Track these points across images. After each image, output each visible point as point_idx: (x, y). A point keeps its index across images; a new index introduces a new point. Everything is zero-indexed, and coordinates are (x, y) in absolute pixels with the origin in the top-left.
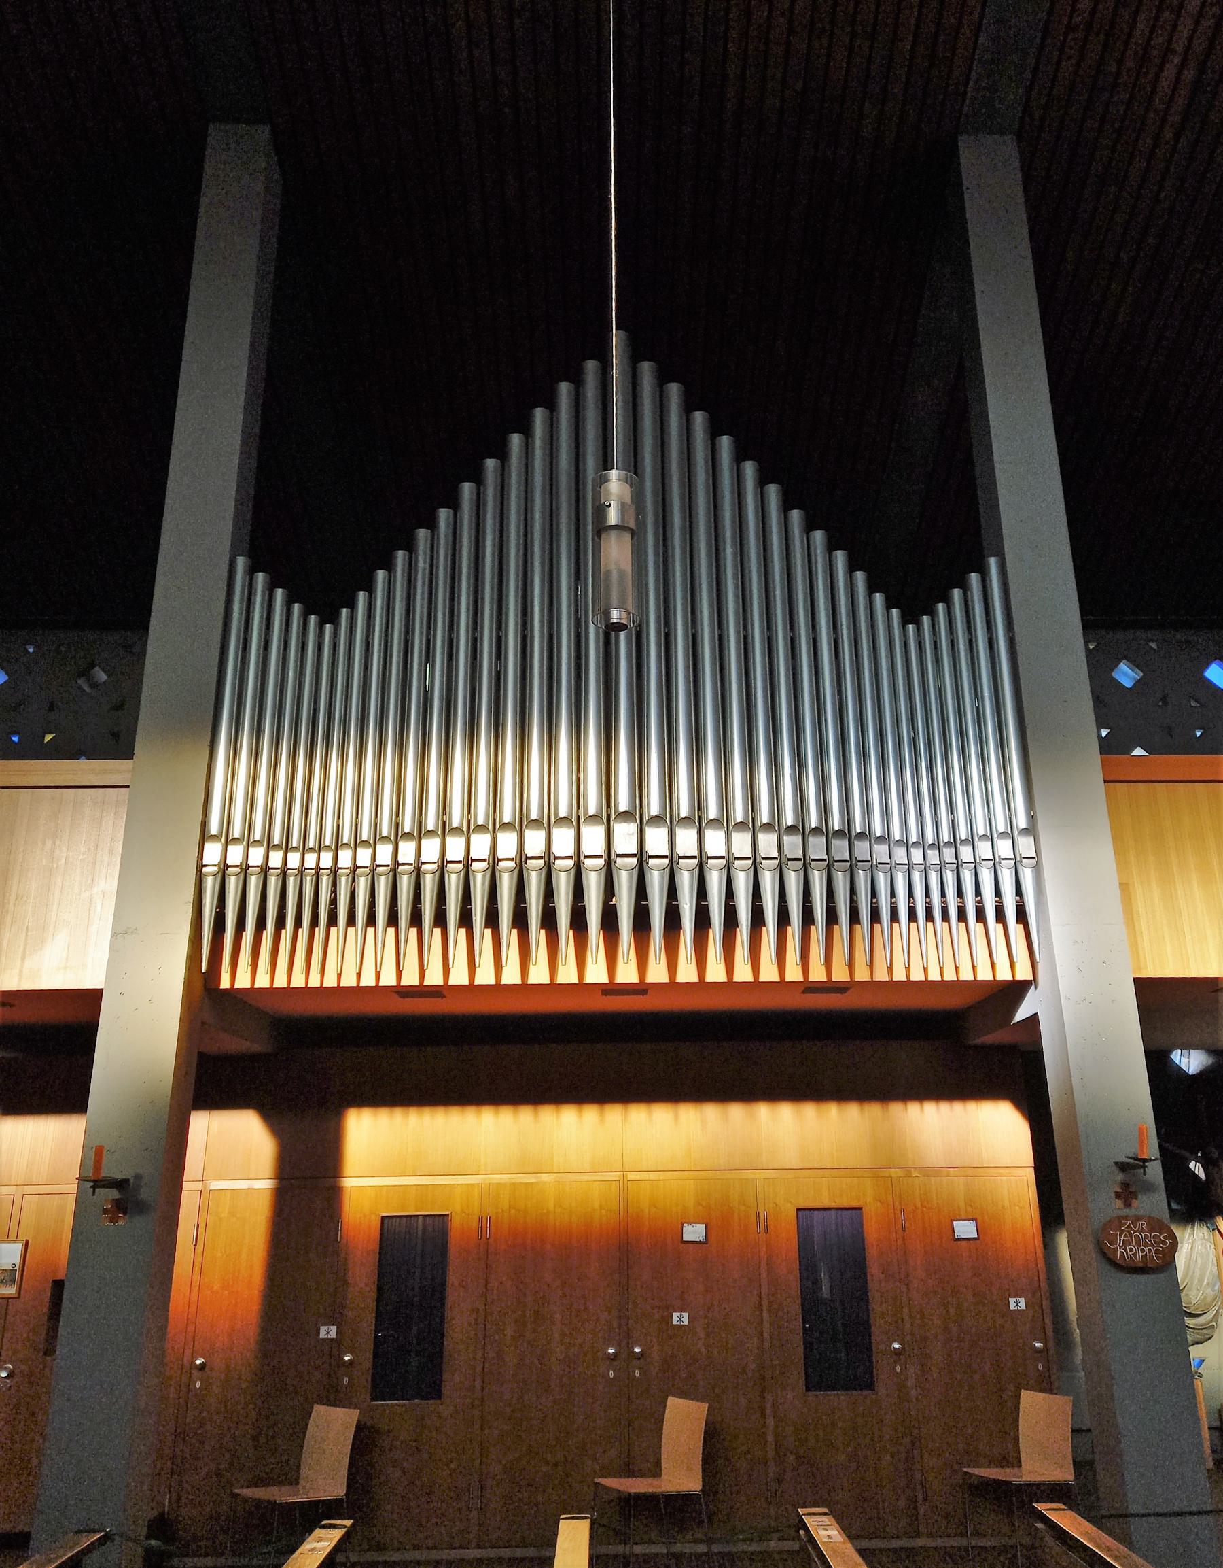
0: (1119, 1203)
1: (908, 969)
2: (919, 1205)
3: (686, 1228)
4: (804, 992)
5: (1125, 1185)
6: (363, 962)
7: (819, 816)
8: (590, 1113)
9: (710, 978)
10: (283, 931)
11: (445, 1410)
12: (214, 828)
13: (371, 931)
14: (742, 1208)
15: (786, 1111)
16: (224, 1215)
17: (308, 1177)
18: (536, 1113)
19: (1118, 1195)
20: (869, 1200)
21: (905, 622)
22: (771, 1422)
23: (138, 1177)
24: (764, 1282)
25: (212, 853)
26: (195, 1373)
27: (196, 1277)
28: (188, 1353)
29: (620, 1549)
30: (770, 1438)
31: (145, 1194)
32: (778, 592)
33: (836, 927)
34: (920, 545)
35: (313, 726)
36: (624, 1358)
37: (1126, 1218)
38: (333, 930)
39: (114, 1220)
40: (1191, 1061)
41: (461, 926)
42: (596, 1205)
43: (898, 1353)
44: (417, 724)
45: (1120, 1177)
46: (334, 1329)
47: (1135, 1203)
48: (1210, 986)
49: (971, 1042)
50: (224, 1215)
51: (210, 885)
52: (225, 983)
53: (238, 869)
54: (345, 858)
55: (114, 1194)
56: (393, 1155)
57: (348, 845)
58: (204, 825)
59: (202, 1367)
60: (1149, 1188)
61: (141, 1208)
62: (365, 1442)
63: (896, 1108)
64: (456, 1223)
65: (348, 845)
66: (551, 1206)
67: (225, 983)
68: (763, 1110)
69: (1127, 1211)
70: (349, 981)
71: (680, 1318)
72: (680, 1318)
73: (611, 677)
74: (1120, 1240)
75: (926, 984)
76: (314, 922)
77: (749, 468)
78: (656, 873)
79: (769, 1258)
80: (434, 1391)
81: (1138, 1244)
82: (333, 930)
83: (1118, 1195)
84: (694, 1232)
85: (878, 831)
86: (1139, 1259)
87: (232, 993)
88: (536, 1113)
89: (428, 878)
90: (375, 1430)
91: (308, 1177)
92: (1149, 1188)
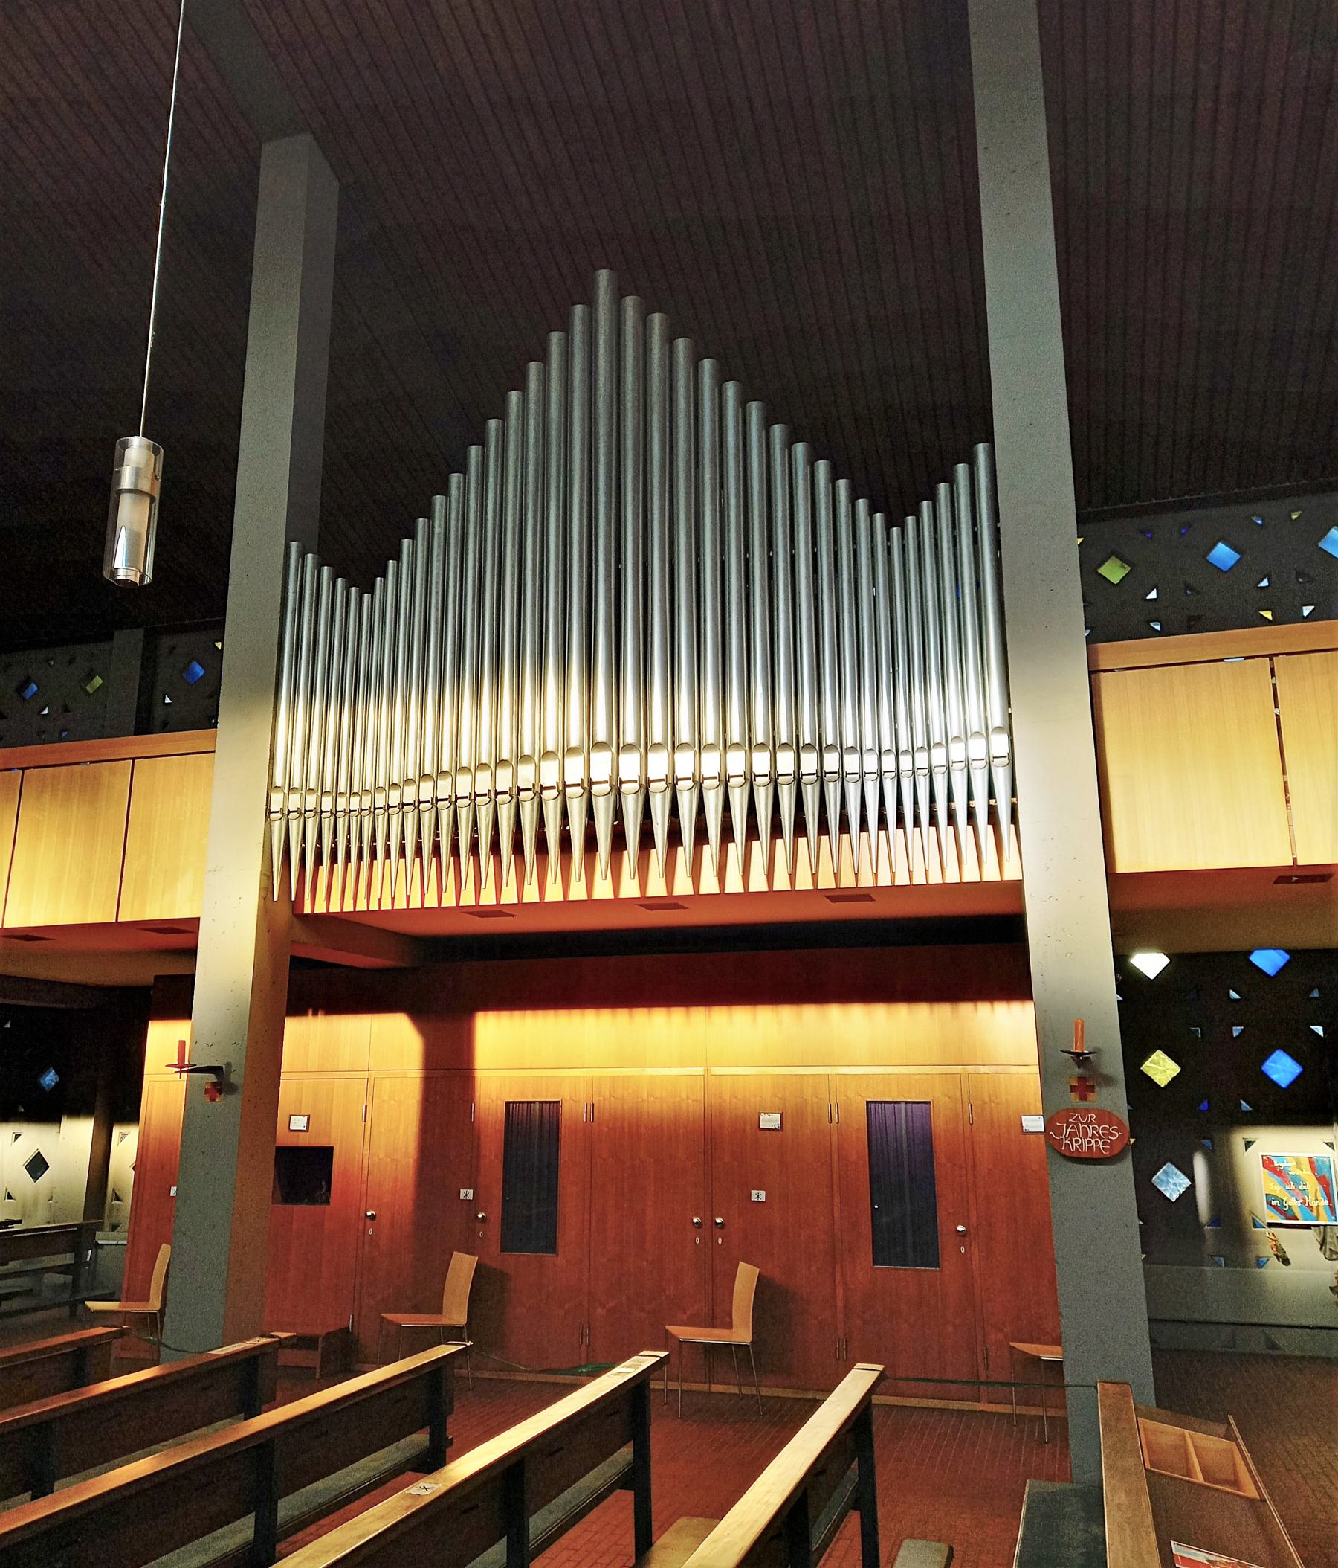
0: (1074, 1096)
1: (815, 877)
2: (987, 1099)
3: (763, 1117)
4: (1276, 882)
5: (1081, 1079)
6: (398, 889)
7: (813, 731)
8: (678, 1014)
9: (704, 890)
10: (680, 849)
11: (560, 1261)
12: (278, 781)
13: (824, 839)
14: (815, 1100)
15: (857, 1013)
16: (386, 1098)
17: (448, 1072)
18: (631, 1015)
19: (207, 1091)
20: (938, 1094)
21: (888, 526)
22: (840, 1291)
23: (228, 1065)
24: (835, 1165)
25: (277, 801)
26: (368, 1222)
27: (367, 1147)
28: (363, 1205)
29: (704, 1387)
30: (840, 1304)
31: (234, 1078)
32: (756, 512)
33: (705, 847)
34: (903, 443)
35: (353, 686)
36: (707, 1227)
37: (1075, 1110)
38: (779, 842)
39: (213, 1100)
40: (1150, 963)
41: (861, 830)
42: (684, 1096)
43: (963, 1234)
44: (434, 676)
45: (1078, 1071)
46: (471, 1191)
47: (1091, 1096)
48: (1318, 875)
49: (970, 948)
50: (386, 1098)
51: (277, 828)
52: (307, 910)
53: (767, 779)
54: (831, 762)
55: (212, 1078)
56: (519, 1052)
57: (939, 744)
58: (271, 777)
59: (373, 1217)
60: (1108, 1081)
61: (232, 1089)
62: (482, 1281)
63: (966, 1009)
64: (566, 1109)
65: (939, 744)
66: (645, 1097)
67: (307, 910)
68: (835, 1012)
69: (1083, 1104)
70: (386, 905)
71: (758, 1195)
72: (758, 1195)
73: (616, 613)
74: (1066, 1132)
75: (910, 889)
76: (334, 859)
77: (731, 389)
78: (809, 787)
79: (840, 1147)
80: (551, 1247)
81: (1085, 1134)
82: (755, 844)
83: (1073, 1089)
84: (770, 1121)
85: (849, 741)
86: (1085, 1148)
87: (315, 917)
88: (631, 1015)
89: (483, 809)
90: (503, 1277)
91: (448, 1072)
92: (1108, 1081)
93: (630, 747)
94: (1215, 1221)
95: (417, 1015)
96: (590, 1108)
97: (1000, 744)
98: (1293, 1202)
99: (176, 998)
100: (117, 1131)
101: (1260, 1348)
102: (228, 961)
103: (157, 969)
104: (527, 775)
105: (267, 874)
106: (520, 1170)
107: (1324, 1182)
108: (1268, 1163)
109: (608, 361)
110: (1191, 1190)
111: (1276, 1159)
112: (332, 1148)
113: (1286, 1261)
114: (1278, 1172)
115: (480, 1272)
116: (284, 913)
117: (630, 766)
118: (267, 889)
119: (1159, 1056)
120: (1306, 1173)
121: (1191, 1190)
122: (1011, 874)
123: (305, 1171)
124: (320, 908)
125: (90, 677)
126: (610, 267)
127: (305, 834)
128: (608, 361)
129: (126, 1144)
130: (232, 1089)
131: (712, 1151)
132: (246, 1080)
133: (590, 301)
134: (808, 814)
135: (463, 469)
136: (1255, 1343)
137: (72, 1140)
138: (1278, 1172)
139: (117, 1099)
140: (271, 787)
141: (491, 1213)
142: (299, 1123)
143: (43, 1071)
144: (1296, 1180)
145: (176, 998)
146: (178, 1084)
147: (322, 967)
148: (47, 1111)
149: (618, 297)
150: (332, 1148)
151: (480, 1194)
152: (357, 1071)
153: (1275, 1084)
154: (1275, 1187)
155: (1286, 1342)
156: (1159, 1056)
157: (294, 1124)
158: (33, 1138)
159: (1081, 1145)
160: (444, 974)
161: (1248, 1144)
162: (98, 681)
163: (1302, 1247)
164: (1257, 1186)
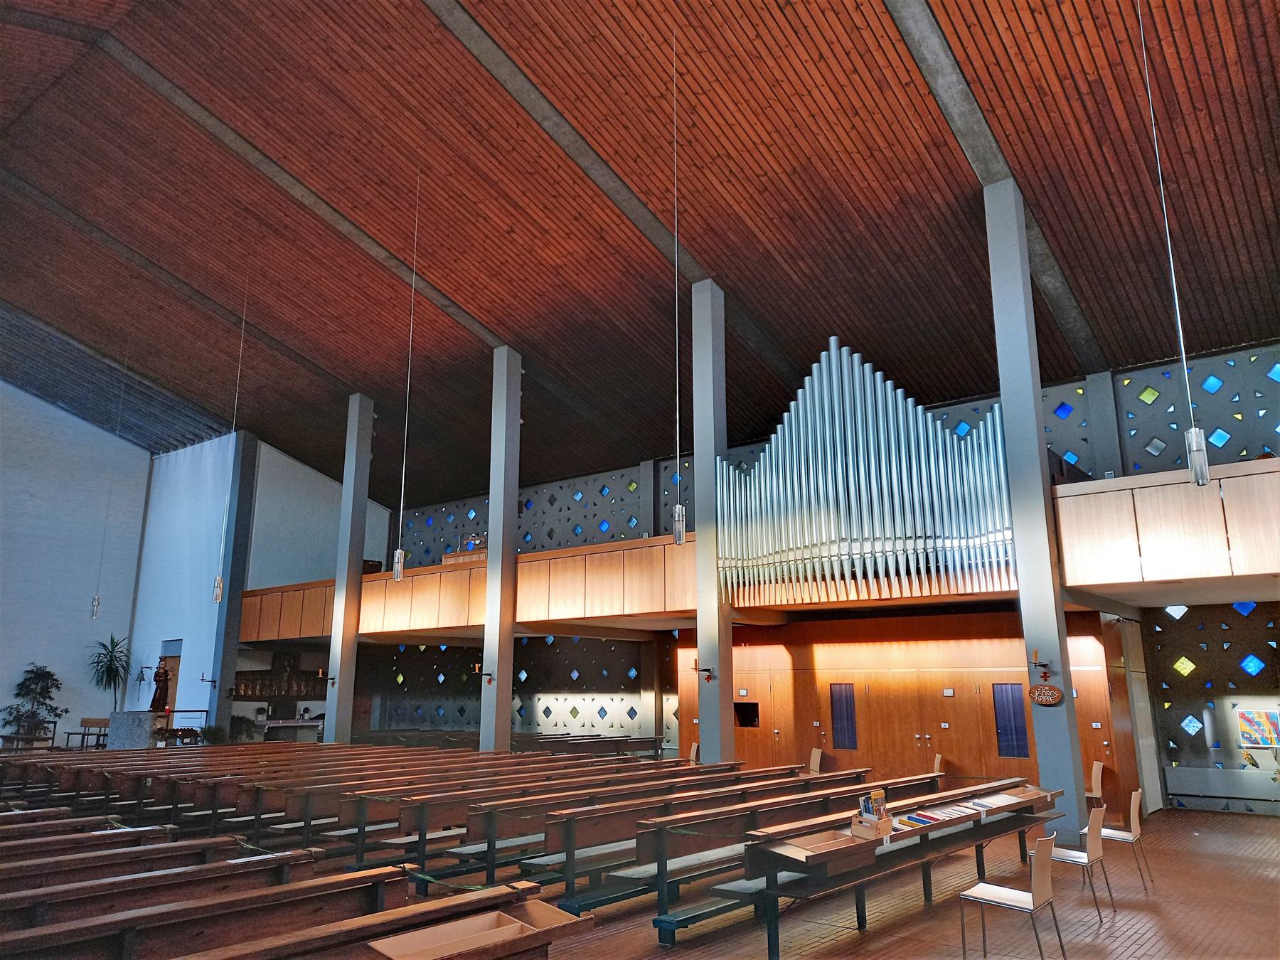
8: (903, 645)
17: (803, 672)
25: (720, 562)
49: (998, 616)
55: (1043, 669)
56: (837, 662)
60: (1055, 674)
61: (715, 678)
64: (856, 687)
68: (975, 644)
91: (803, 672)
92: (1055, 674)
93: (856, 540)
94: (1217, 744)
95: (788, 644)
96: (867, 687)
97: (1008, 534)
98: (1257, 736)
99: (689, 638)
100: (665, 697)
101: (1243, 810)
102: (709, 625)
103: (682, 631)
104: (816, 551)
105: (720, 593)
106: (841, 712)
107: (1275, 725)
108: (1242, 716)
109: (839, 381)
110: (1202, 729)
111: (1250, 714)
112: (756, 705)
113: (1255, 765)
114: (1250, 721)
115: (823, 756)
116: (727, 607)
117: (856, 548)
118: (720, 599)
119: (1183, 660)
120: (1264, 720)
121: (1202, 729)
122: (1014, 587)
123: (747, 713)
124: (741, 605)
125: (630, 484)
126: (835, 335)
127: (732, 576)
128: (839, 381)
129: (671, 703)
130: (715, 678)
131: (922, 706)
132: (717, 673)
133: (827, 349)
134: (931, 568)
135: (782, 423)
136: (1239, 807)
137: (646, 701)
138: (1250, 721)
139: (667, 682)
140: (718, 558)
141: (828, 732)
142: (743, 692)
143: (629, 669)
144: (1259, 724)
145: (689, 638)
146: (695, 676)
147: (747, 628)
148: (633, 687)
149: (840, 346)
150: (756, 705)
151: (822, 723)
152: (765, 670)
153: (1249, 674)
154: (1247, 728)
155: (1259, 808)
156: (1183, 660)
157: (742, 694)
158: (628, 700)
159: (1044, 699)
160: (799, 628)
161: (1234, 706)
162: (634, 485)
163: (1266, 759)
164: (1238, 727)
